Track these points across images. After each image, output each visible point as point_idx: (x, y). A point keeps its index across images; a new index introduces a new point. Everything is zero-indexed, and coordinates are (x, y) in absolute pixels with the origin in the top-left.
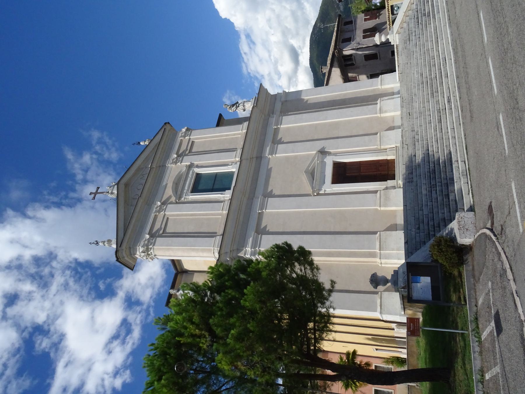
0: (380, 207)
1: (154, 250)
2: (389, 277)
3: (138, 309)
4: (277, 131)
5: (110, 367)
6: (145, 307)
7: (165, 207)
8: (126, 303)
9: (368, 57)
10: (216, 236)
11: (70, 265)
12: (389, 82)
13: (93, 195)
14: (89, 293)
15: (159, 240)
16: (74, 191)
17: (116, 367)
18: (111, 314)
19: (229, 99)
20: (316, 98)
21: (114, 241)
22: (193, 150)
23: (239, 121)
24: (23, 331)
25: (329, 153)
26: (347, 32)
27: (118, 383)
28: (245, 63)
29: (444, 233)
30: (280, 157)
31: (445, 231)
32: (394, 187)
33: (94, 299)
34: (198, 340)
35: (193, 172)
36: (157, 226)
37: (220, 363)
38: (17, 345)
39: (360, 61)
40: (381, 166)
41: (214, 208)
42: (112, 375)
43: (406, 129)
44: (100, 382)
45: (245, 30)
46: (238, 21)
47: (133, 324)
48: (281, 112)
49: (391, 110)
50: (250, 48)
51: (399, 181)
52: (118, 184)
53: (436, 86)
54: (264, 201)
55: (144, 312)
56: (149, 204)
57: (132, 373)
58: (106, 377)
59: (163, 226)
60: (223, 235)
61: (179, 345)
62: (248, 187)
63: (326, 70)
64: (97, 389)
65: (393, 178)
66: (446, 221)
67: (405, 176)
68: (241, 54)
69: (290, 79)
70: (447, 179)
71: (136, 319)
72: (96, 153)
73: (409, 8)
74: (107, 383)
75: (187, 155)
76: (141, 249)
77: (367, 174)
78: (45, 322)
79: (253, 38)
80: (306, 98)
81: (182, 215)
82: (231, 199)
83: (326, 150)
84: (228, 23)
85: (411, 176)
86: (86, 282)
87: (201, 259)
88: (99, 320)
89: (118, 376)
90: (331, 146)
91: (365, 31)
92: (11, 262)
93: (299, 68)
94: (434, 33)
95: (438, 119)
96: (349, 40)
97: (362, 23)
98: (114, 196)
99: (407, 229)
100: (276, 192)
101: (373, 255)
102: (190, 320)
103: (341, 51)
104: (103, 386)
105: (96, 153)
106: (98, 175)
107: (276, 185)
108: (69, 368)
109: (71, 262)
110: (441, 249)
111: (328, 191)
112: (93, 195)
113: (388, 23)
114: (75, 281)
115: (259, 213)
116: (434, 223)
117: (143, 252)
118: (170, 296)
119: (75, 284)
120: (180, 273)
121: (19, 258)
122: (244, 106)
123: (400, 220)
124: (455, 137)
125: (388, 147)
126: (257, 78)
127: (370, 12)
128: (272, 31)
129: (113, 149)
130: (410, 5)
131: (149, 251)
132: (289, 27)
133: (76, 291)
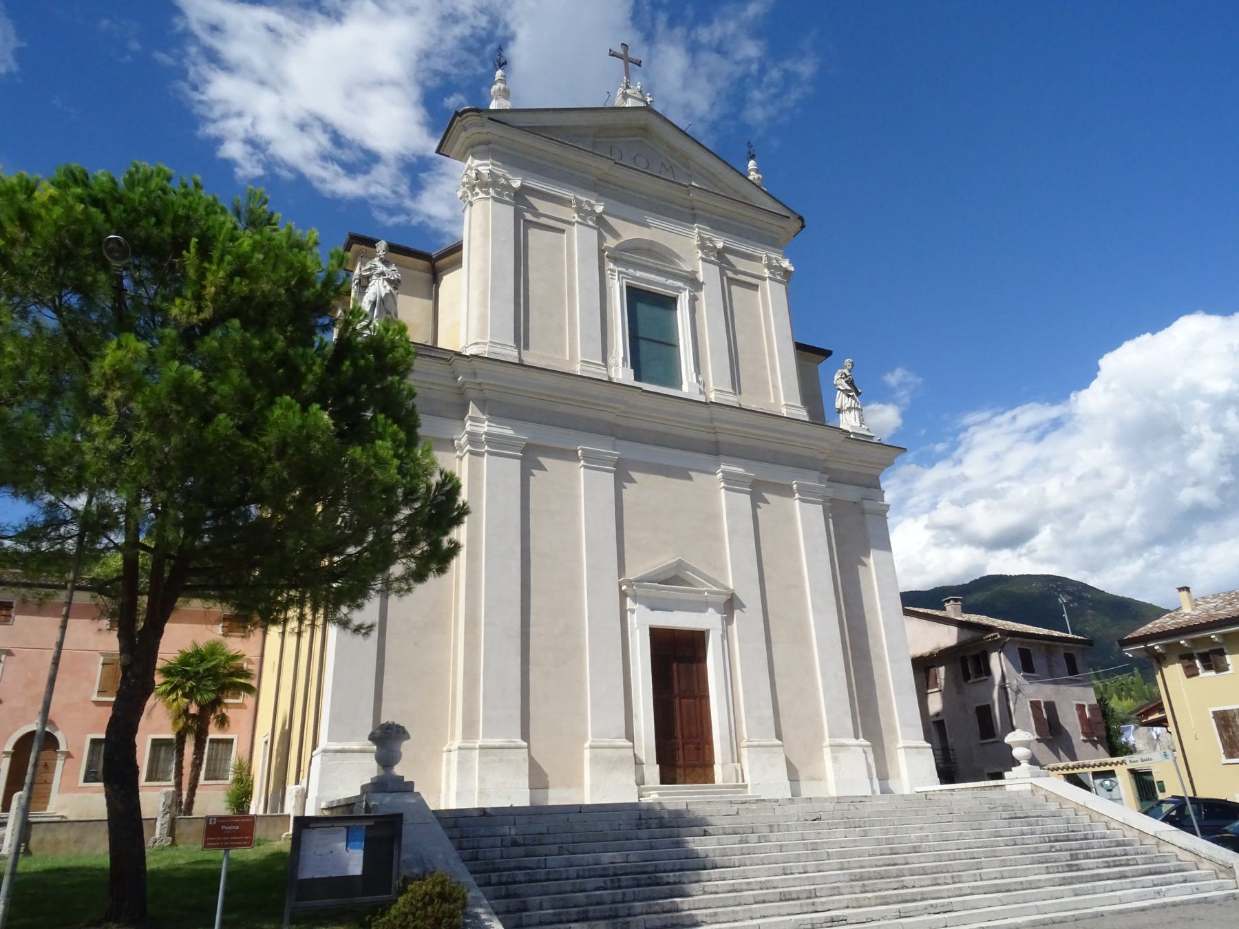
0: (592, 747)
1: (482, 202)
2: (398, 770)
3: (404, 189)
4: (785, 491)
5: (268, 129)
6: (408, 203)
7: (590, 223)
8: (415, 160)
9: (984, 713)
10: (518, 347)
11: (501, 26)
12: (914, 766)
13: (620, 51)
14: (436, 73)
15: (509, 211)
16: (671, 24)
17: (268, 143)
18: (392, 125)
19: (902, 384)
20: (872, 588)
21: (506, 105)
22: (734, 288)
23: (813, 396)
25: (728, 621)
26: (1049, 660)
27: (233, 150)
28: (991, 418)
29: (480, 910)
30: (718, 498)
31: (487, 913)
32: (640, 782)
33: (422, 84)
34: (189, 294)
35: (678, 289)
37: (119, 346)
39: (974, 691)
40: (698, 749)
41: (583, 339)
42: (252, 134)
43: (779, 811)
44: (234, 109)
45: (1071, 416)
46: (1091, 400)
47: (368, 178)
48: (832, 500)
49: (841, 772)
50: (1028, 430)
51: (659, 795)
52: (648, 108)
53: (880, 887)
54: (605, 461)
55: (398, 201)
56: (597, 187)
57: (257, 181)
58: (247, 121)
59: (542, 220)
60: (521, 364)
61: (180, 244)
62: (635, 424)
63: (952, 610)
64: (219, 101)
65: (666, 779)
66: (517, 915)
67: (658, 808)
68: (1013, 407)
69: (954, 528)
70: (629, 915)
71: (378, 185)
72: (763, 71)
73: (1096, 817)
74: (233, 124)
75: (722, 274)
76: (484, 170)
77: (678, 714)
79: (1053, 437)
81: (571, 266)
82: (610, 382)
83: (737, 613)
84: (1086, 375)
85: (654, 822)
86: (461, 64)
87: (463, 316)
88: (376, 99)
89: (249, 149)
90: (746, 623)
91: (1051, 706)
93: (982, 550)
94: (1021, 883)
95: (790, 893)
96: (1027, 666)
97: (1073, 700)
98: (618, 102)
99: (536, 812)
100: (629, 492)
101: (469, 730)
102: (241, 270)
103: (999, 646)
104: (225, 116)
105: (763, 71)
106: (711, 78)
107: (647, 490)
108: (264, 36)
109: (506, 26)
110: (431, 901)
111: (632, 620)
112: (620, 51)
113: (1071, 764)
114: (463, 40)
115: (576, 451)
116: (521, 882)
117: (478, 174)
118: (371, 243)
119: (455, 37)
120: (433, 266)
122: (850, 409)
123: (557, 797)
125: (744, 766)
126: (955, 446)
127: (1100, 718)
128: (1071, 482)
129: (772, 111)
130: (1105, 819)
131: (480, 188)
132: (1083, 523)
133: (441, 41)
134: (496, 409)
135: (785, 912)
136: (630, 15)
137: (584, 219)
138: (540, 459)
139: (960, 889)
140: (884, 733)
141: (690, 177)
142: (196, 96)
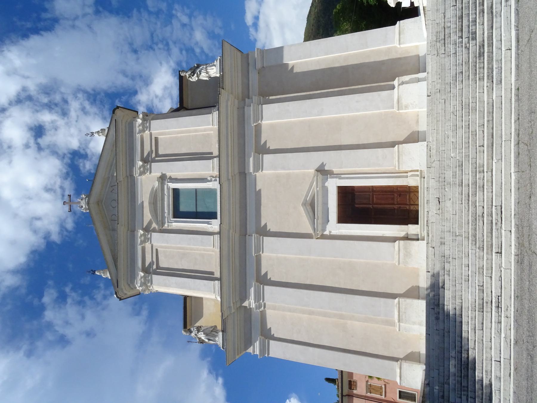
16: (45, 10)
24: (64, 158)
30: (269, 173)
35: (168, 189)
36: (148, 261)
38: (65, 171)
54: (259, 240)
78: (79, 147)
80: (291, 63)
92: (18, 95)
94: (488, 121)
95: (479, 304)
111: (334, 232)
121: (24, 89)
122: (207, 73)
123: (422, 348)
124: (500, 378)
133: (96, 114)
134: (244, 296)
135: (490, 324)
136: (49, 32)
137: (147, 128)
138: (262, 144)
139: (487, 181)
140: (390, 57)
141: (113, 176)
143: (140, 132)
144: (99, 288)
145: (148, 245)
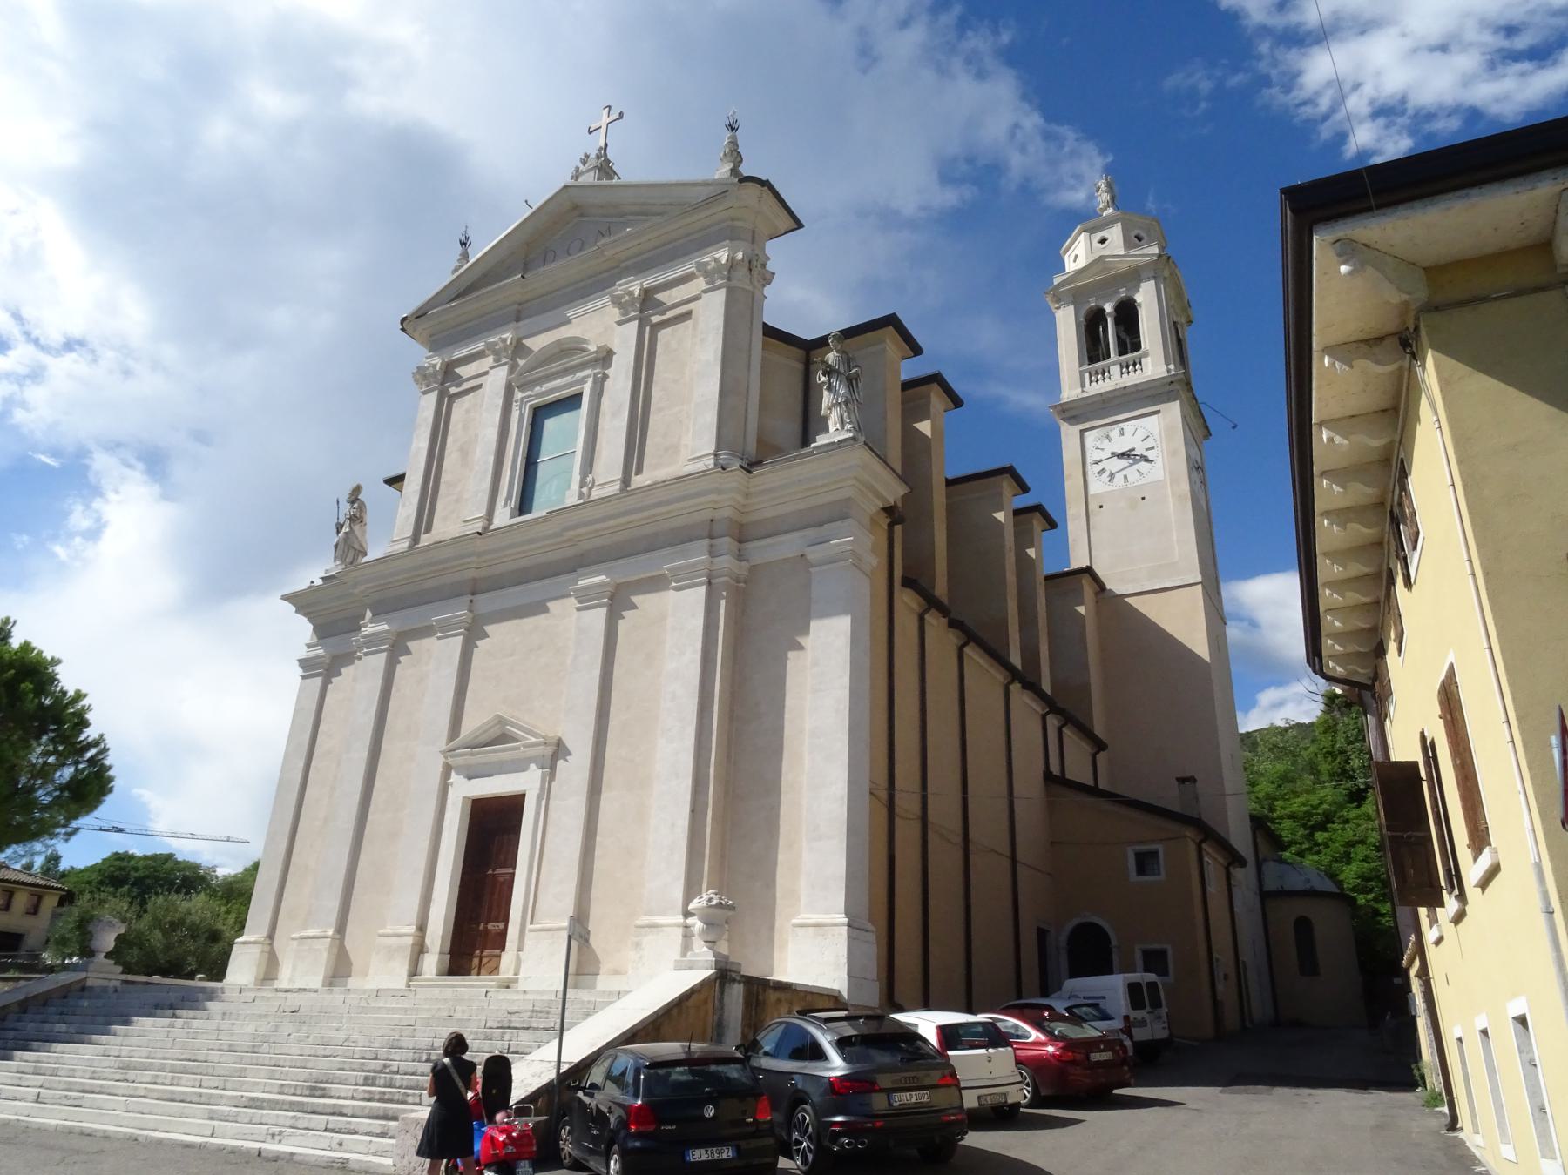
17: (1403, 100)
89: (1381, 121)
142: (1297, 95)
143: (702, 267)
144: (996, 32)
145: (700, 283)
